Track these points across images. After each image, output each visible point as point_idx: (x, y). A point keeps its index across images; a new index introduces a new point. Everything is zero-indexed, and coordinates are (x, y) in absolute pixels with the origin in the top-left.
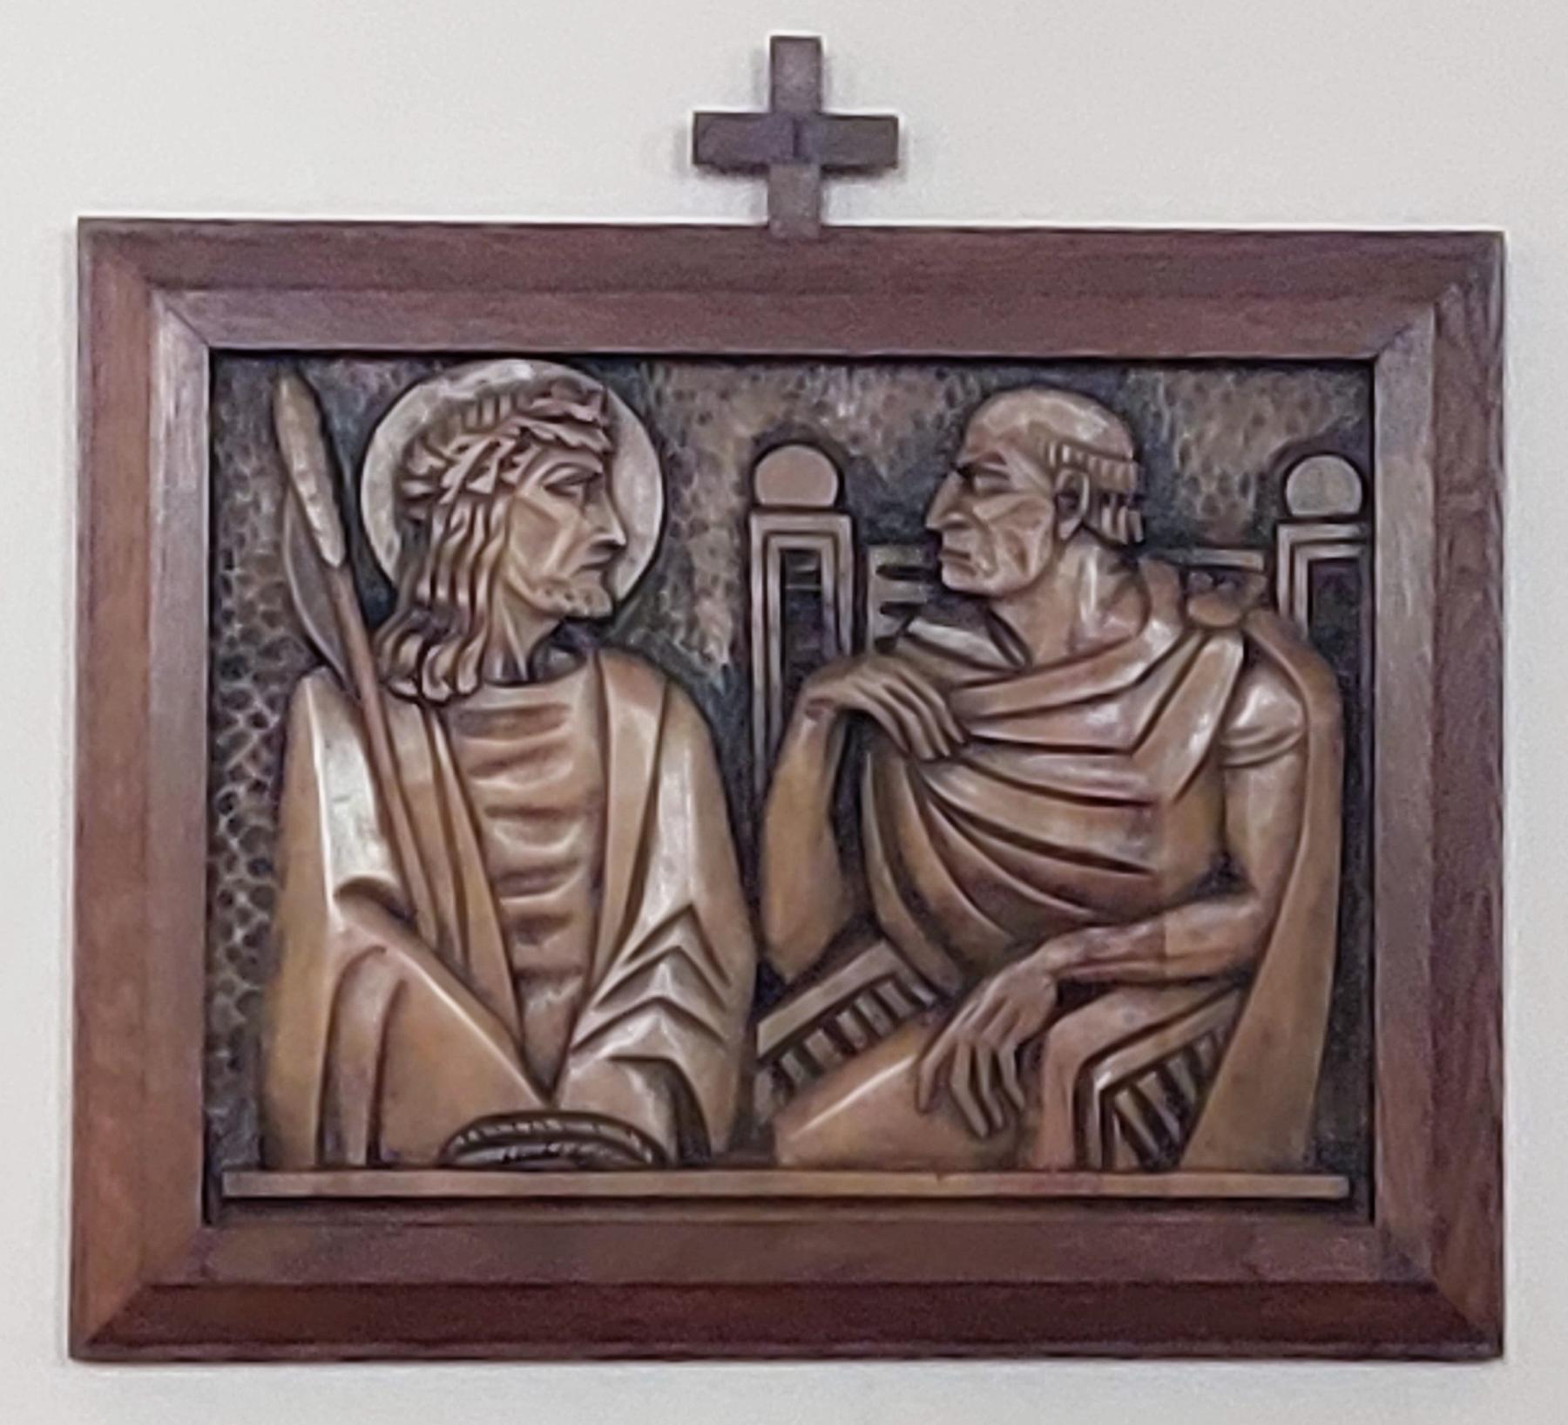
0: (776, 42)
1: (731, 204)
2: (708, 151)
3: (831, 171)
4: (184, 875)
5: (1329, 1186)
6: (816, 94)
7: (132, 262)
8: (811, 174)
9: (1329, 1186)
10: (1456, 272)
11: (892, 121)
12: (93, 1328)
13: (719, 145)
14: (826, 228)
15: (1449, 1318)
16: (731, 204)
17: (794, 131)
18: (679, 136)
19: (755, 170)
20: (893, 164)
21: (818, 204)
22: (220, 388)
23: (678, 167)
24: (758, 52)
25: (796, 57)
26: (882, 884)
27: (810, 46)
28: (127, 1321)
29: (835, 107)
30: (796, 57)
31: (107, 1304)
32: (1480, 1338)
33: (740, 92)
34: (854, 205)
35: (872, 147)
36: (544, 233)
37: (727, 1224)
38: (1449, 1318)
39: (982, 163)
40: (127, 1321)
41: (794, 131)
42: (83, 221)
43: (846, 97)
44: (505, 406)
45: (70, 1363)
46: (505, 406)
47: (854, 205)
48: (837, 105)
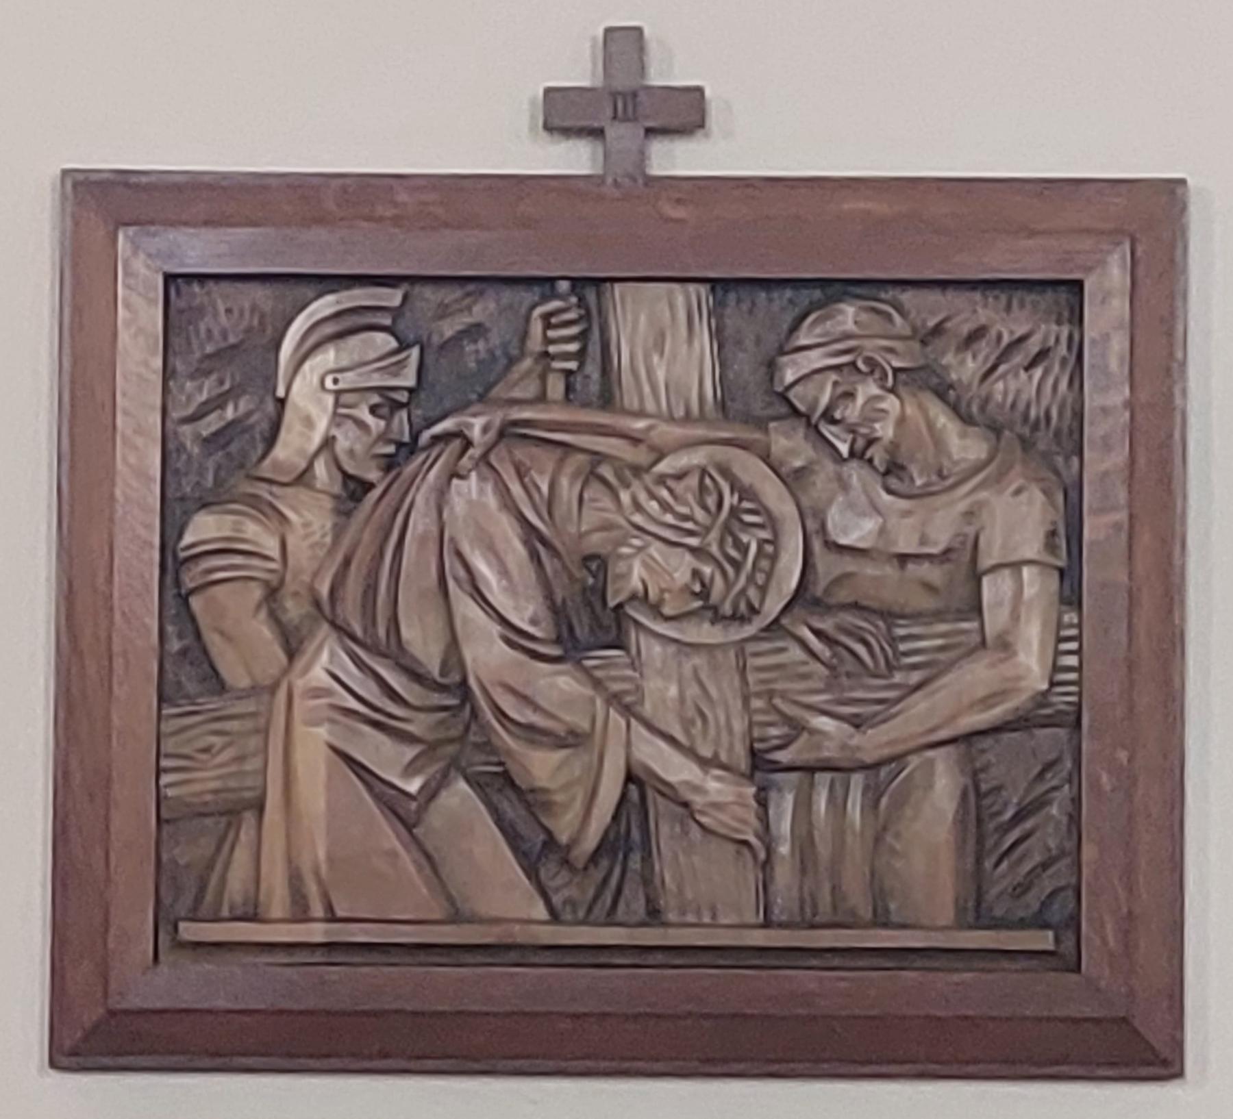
1: (573, 159)
3: (650, 132)
4: (146, 668)
5: (1044, 940)
7: (104, 204)
9: (1044, 940)
10: (1149, 217)
11: (699, 90)
13: (563, 114)
14: (651, 181)
15: (1144, 1048)
16: (573, 159)
17: (626, 101)
18: (533, 102)
19: (597, 133)
20: (701, 125)
22: (176, 341)
23: (532, 129)
24: (594, 39)
25: (623, 44)
28: (95, 1032)
30: (623, 44)
32: (1165, 1063)
33: (579, 72)
34: (676, 159)
35: (686, 113)
36: (998, 185)
37: (634, 1059)
38: (1144, 1048)
39: (772, 126)
40: (95, 1032)
41: (626, 101)
42: (65, 173)
44: (765, 534)
45: (52, 1072)
46: (765, 534)
47: (676, 159)
48: (656, 79)
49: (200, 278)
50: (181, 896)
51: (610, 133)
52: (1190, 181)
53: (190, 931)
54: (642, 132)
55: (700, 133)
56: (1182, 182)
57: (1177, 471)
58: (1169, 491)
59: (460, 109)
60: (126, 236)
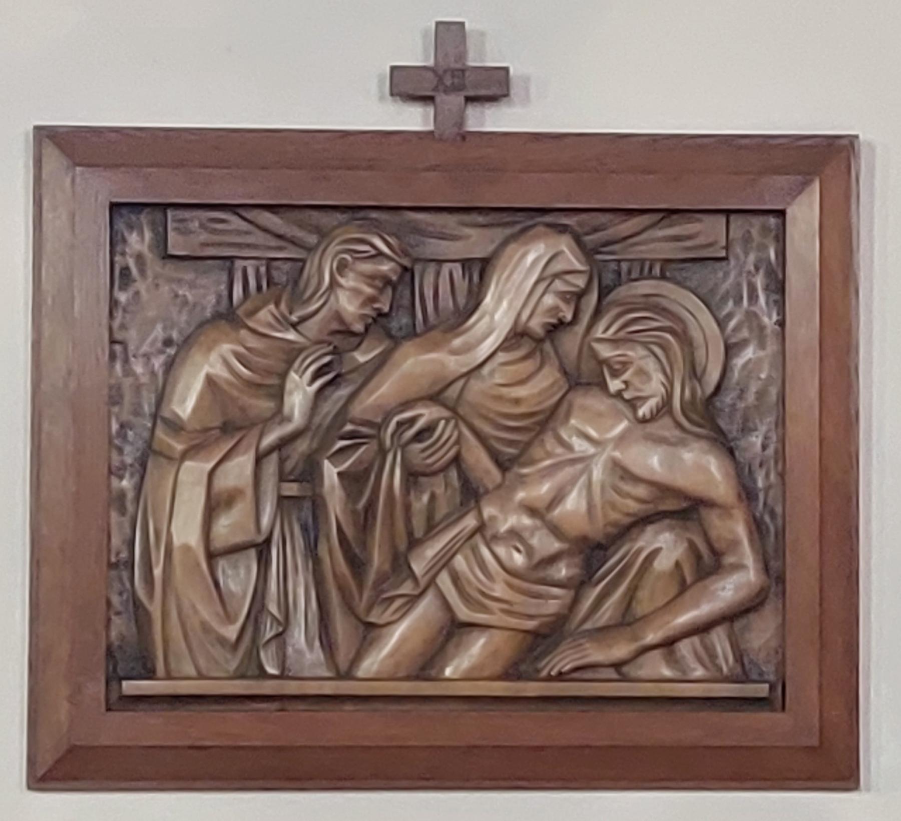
0: (393, 69)
1: (414, 119)
2: (395, 91)
3: (469, 100)
6: (462, 56)
7: (65, 147)
8: (458, 99)
12: (40, 773)
13: (405, 85)
14: (465, 136)
15: (833, 763)
16: (414, 119)
17: (452, 77)
19: (427, 99)
20: (506, 95)
21: (461, 123)
23: (382, 98)
25: (450, 34)
26: (150, 405)
27: (395, 73)
28: (58, 767)
29: (471, 63)
30: (450, 34)
31: (47, 760)
33: (416, 54)
35: (495, 87)
38: (833, 763)
39: (575, 90)
40: (58, 767)
41: (452, 77)
43: (485, 55)
49: (160, 203)
50: (135, 656)
51: (440, 98)
52: (861, 137)
53: (130, 687)
54: (462, 100)
55: (505, 99)
56: (857, 137)
57: (854, 220)
58: (851, 251)
59: (346, 95)
60: (184, 411)
